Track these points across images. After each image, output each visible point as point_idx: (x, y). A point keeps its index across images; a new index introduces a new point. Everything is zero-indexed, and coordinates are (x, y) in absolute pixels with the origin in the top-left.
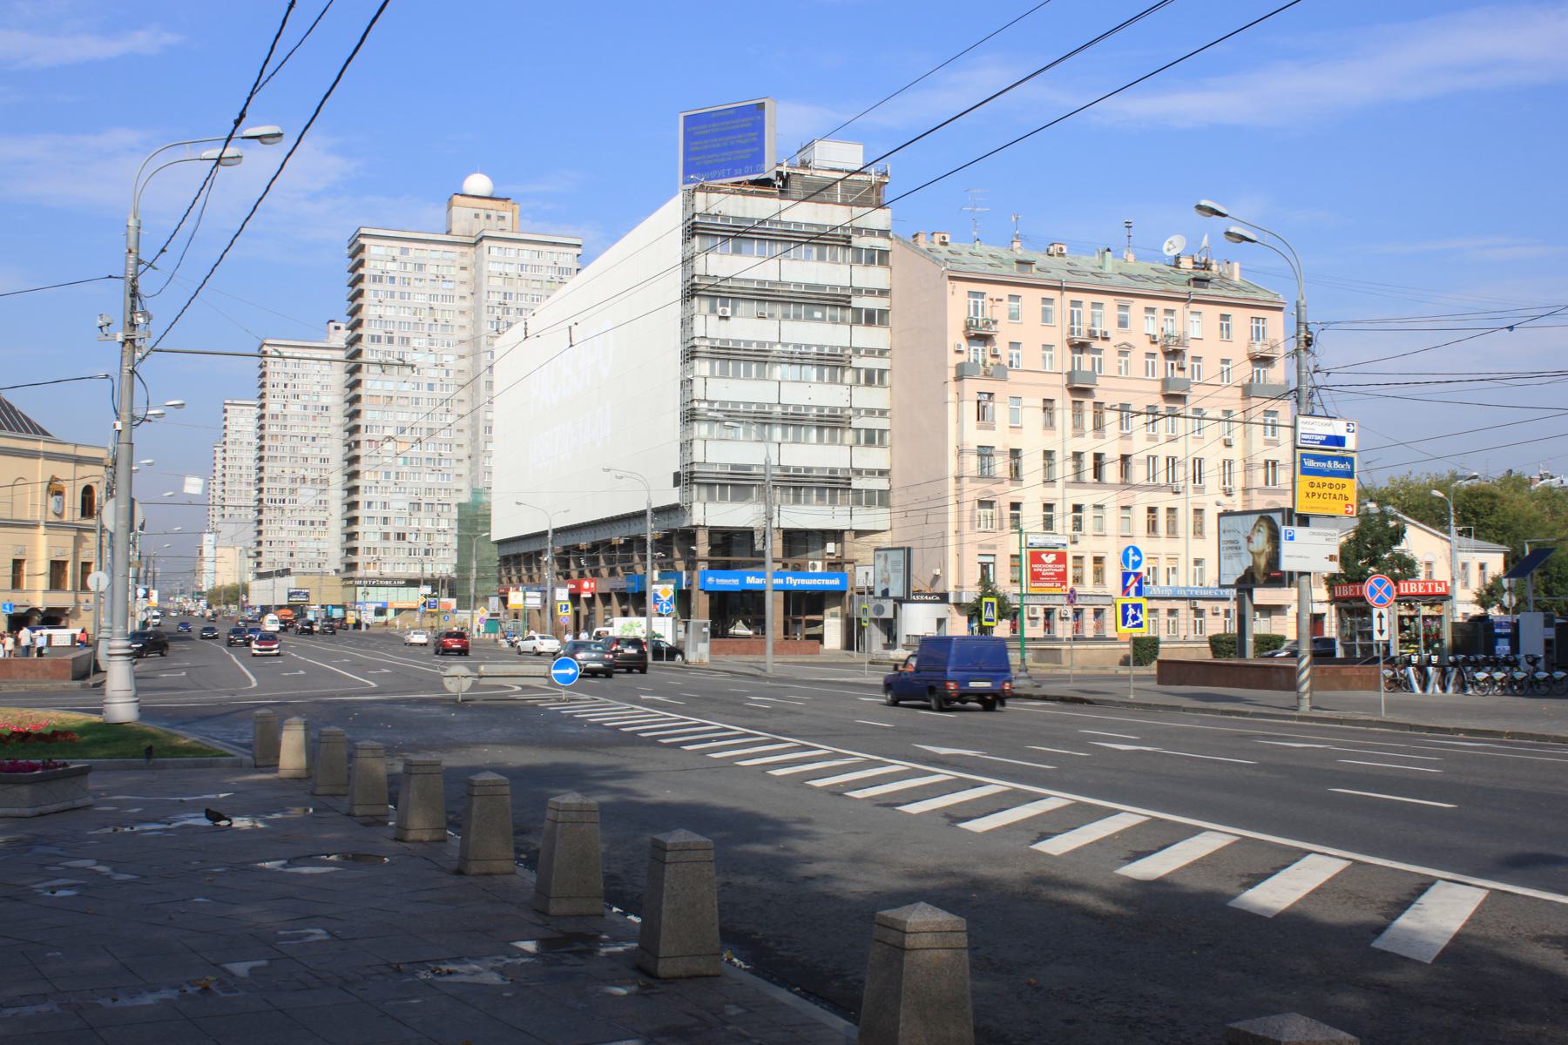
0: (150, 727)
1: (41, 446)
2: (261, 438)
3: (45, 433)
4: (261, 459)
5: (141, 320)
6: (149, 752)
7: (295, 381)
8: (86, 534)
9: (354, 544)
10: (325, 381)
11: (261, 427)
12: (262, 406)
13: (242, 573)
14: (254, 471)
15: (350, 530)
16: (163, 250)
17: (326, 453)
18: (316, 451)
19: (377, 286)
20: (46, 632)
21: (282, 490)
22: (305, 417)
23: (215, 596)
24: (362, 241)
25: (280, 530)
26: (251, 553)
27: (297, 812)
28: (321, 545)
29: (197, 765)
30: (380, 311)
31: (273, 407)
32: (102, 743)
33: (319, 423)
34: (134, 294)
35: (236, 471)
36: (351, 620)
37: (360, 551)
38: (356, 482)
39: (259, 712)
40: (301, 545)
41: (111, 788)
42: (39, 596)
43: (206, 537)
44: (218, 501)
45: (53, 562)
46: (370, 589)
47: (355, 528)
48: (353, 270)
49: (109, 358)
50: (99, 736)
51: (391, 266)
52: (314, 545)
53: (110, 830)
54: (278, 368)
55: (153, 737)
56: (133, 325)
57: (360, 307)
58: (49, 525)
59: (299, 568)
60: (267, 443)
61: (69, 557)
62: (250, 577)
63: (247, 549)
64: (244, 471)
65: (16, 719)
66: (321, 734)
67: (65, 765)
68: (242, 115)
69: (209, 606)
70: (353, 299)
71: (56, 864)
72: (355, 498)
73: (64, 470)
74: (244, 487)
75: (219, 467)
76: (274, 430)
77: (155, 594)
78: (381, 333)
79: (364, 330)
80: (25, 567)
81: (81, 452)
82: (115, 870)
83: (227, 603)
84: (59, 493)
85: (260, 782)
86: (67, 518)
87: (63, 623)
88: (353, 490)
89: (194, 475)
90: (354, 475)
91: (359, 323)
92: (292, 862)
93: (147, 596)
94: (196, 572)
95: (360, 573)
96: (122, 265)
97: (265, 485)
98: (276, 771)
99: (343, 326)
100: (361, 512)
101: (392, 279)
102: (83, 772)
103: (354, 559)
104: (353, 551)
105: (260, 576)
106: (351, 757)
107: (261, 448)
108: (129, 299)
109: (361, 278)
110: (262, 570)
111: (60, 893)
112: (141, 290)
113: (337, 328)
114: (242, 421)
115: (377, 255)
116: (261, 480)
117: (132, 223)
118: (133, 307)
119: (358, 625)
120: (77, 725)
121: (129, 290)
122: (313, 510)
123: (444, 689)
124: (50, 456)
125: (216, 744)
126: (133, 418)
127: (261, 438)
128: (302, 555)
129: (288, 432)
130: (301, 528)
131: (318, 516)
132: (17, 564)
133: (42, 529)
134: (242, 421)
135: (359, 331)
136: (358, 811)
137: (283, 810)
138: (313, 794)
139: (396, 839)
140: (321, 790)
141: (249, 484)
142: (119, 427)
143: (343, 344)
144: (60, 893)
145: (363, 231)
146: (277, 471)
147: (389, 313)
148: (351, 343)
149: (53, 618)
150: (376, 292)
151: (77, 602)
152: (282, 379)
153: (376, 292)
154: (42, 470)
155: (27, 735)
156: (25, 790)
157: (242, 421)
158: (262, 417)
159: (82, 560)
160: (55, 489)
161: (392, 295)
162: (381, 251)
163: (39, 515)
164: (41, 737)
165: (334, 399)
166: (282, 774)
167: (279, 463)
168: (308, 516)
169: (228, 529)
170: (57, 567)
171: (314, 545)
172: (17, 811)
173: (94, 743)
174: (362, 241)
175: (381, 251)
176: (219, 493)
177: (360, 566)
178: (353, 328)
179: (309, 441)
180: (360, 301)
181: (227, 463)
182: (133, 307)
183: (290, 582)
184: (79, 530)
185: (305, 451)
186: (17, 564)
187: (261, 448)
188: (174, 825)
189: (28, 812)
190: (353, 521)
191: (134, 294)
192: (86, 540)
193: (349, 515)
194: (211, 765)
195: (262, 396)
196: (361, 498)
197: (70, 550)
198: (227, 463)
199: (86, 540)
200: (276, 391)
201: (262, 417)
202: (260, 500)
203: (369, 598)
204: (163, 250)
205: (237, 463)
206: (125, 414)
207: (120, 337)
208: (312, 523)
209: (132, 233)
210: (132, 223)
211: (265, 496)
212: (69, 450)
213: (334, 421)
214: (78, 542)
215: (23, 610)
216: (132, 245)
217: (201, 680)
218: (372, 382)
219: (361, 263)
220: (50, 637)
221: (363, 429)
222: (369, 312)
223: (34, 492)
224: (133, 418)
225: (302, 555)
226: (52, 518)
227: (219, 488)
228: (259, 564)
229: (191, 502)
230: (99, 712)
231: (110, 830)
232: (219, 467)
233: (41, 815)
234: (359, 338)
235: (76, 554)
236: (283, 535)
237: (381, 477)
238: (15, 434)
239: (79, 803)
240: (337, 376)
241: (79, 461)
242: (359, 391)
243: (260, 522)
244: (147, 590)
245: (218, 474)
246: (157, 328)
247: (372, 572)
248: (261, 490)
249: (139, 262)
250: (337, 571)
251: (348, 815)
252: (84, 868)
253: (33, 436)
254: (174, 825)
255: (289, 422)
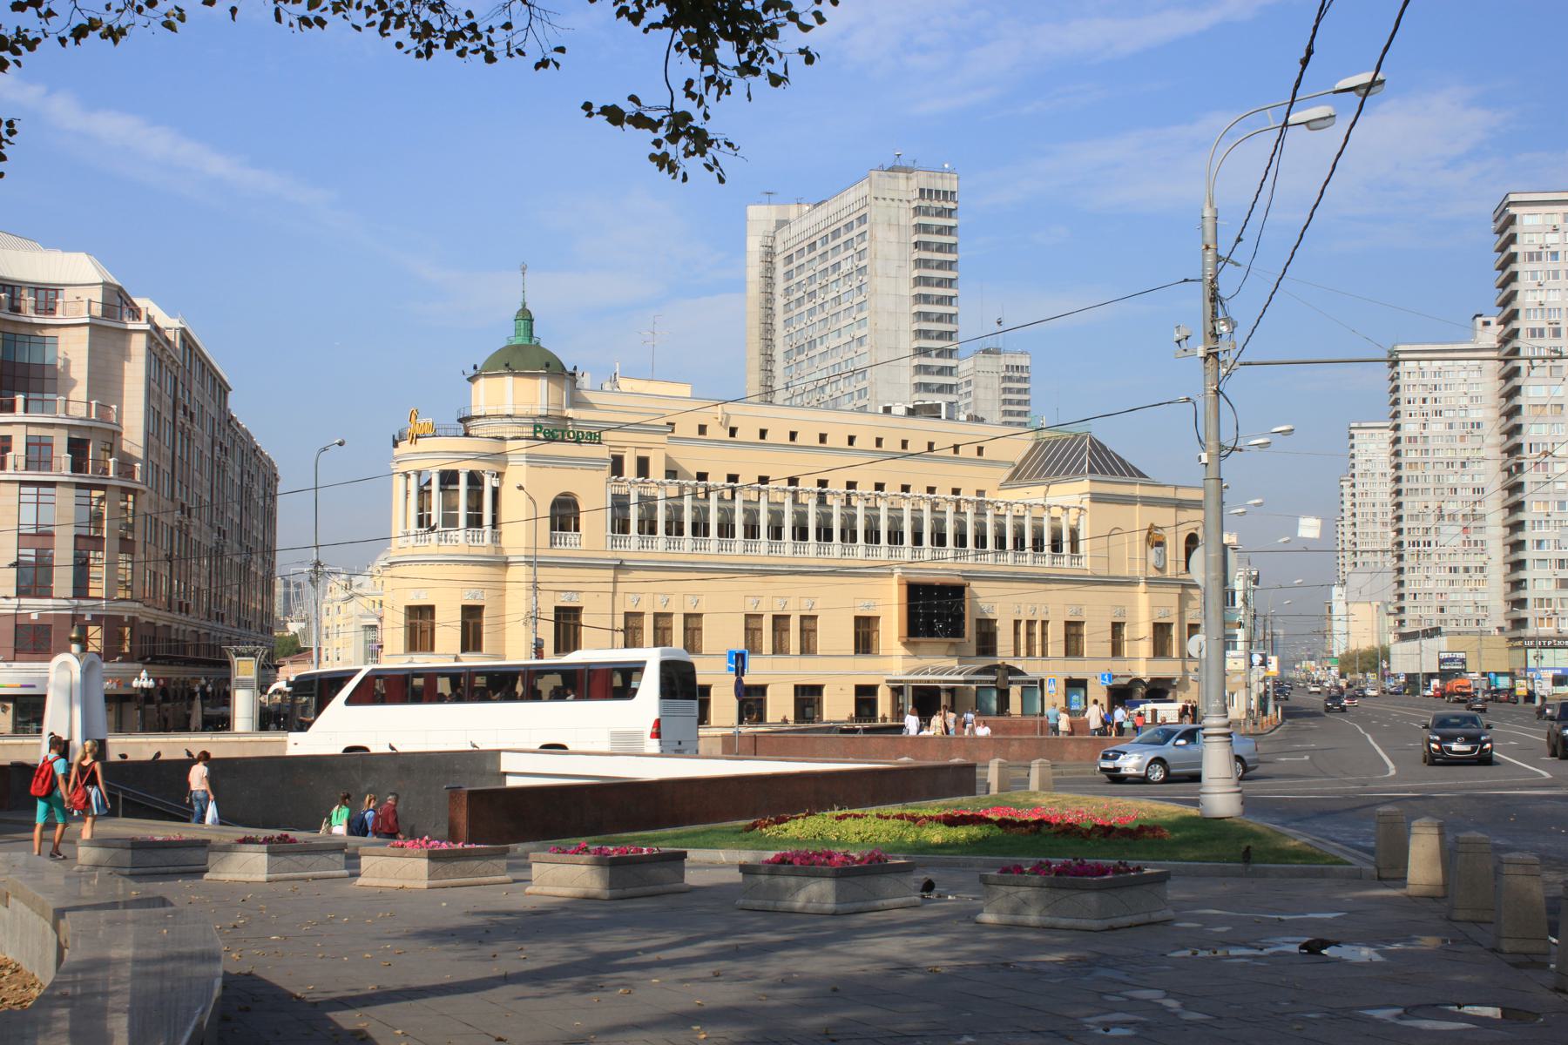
0: (1256, 824)
1: (1138, 490)
2: (1398, 467)
3: (1142, 475)
4: (1398, 492)
5: (1224, 329)
6: (1247, 856)
7: (1436, 394)
8: (1192, 591)
9: (1522, 594)
10: (1474, 391)
11: (1397, 454)
12: (1397, 428)
13: (1381, 634)
14: (1390, 508)
15: (1515, 577)
16: (1239, 240)
17: (1480, 481)
18: (1467, 479)
19: (1535, 266)
20: (1150, 706)
21: (1427, 530)
22: (1452, 438)
23: (1349, 662)
24: (1512, 210)
25: (1426, 580)
26: (1391, 609)
27: (1429, 942)
28: (1479, 597)
29: (1306, 874)
30: (1541, 296)
31: (1410, 428)
32: (1194, 842)
33: (1469, 444)
34: (1215, 298)
35: (1369, 509)
36: (1521, 691)
37: (1530, 603)
38: (1521, 516)
39: (1381, 809)
40: (1453, 597)
41: (1196, 899)
42: (1141, 664)
43: (1336, 590)
44: (1347, 546)
45: (1156, 625)
46: (1545, 652)
47: (1522, 575)
48: (1502, 249)
49: (1193, 378)
50: (1194, 832)
51: (1552, 238)
52: (1470, 597)
53: (1188, 953)
54: (1414, 379)
55: (1256, 836)
56: (1215, 336)
57: (1514, 294)
58: (1150, 582)
59: (1452, 627)
60: (1404, 472)
61: (1174, 619)
62: (1391, 638)
63: (1386, 604)
64: (1378, 509)
65: (1102, 810)
66: (1457, 841)
67: (1139, 869)
68: (1310, 52)
69: (1342, 676)
70: (1503, 286)
71: (1117, 993)
72: (1520, 536)
73: (1163, 517)
74: (1379, 529)
75: (1347, 505)
76: (1412, 456)
77: (1274, 661)
78: (1544, 325)
79: (1521, 324)
80: (1125, 631)
81: (1183, 495)
82: (1184, 1006)
83: (1364, 672)
84: (1160, 544)
85: (1383, 898)
86: (1170, 572)
87: (1170, 696)
88: (1518, 526)
89: (1309, 514)
90: (1517, 507)
91: (1514, 315)
92: (1409, 1012)
93: (1264, 663)
94: (1325, 634)
95: (1530, 631)
96: (1198, 264)
97: (1404, 525)
98: (1404, 886)
99: (1493, 321)
100: (1529, 554)
101: (1555, 255)
102: (1161, 879)
103: (1523, 614)
104: (1521, 603)
105: (1404, 637)
106: (1498, 873)
107: (1398, 479)
108: (1208, 304)
109: (1513, 258)
110: (1406, 630)
111: (1114, 1032)
112: (1221, 293)
113: (1487, 324)
114: (1372, 447)
115: (1532, 226)
116: (1399, 518)
117: (1208, 213)
118: (1215, 314)
119: (1530, 697)
120: (1171, 818)
121: (1209, 294)
122: (1466, 553)
123: (602, 861)
124: (1148, 501)
125: (1332, 848)
126: (1221, 447)
127: (1398, 467)
128: (1455, 611)
129: (1430, 457)
130: (1453, 576)
131: (1474, 561)
132: (1117, 628)
133: (1142, 587)
134: (1373, 447)
135: (1515, 325)
136: (1506, 946)
137: (1407, 939)
138: (1449, 919)
139: (1557, 990)
140: (1460, 915)
141: (1384, 524)
142: (1205, 459)
143: (1494, 343)
144: (1114, 1032)
145: (1512, 198)
146: (1419, 507)
147: (1553, 299)
148: (1504, 341)
149: (1159, 690)
150: (1534, 274)
151: (1185, 671)
152: (1418, 393)
153: (1534, 274)
154: (1140, 517)
155: (1111, 829)
156: (1092, 898)
157: (1373, 447)
158: (1397, 441)
159: (1188, 621)
160: (1155, 540)
161: (1556, 276)
162: (1537, 220)
163: (1138, 571)
164: (1126, 832)
165: (1487, 413)
166: (1411, 890)
167: (1420, 497)
168: (1460, 561)
169: (1355, 580)
170: (1161, 631)
171: (1470, 597)
172: (1084, 923)
173: (1184, 842)
174: (1512, 210)
175: (1537, 220)
176: (1348, 536)
177: (1531, 623)
178: (1505, 321)
179: (1457, 467)
180: (1513, 286)
181: (1357, 500)
182: (1215, 314)
183: (1441, 643)
184: (1184, 586)
185: (1452, 480)
186: (1117, 628)
187: (1398, 479)
188: (1266, 951)
189: (1095, 924)
190: (1519, 565)
191: (1215, 298)
192: (1192, 598)
193: (1513, 558)
194: (1322, 874)
195: (1396, 415)
196: (1528, 535)
197: (1175, 610)
198: (1357, 500)
199: (1192, 598)
200: (1412, 408)
201: (1397, 441)
202: (1400, 544)
203: (1544, 663)
204: (1239, 240)
205: (1369, 500)
206: (1212, 443)
207: (1201, 352)
208: (1467, 570)
209: (1209, 225)
210: (1208, 213)
211: (1405, 538)
212: (1168, 493)
213: (1489, 441)
214: (1183, 600)
215: (1125, 681)
216: (1209, 239)
217: (1308, 772)
218: (1534, 390)
219: (1512, 239)
220: (1154, 712)
221: (1526, 448)
222: (1526, 298)
223: (1132, 542)
224: (1221, 447)
225: (1455, 611)
226: (1153, 573)
227: (1348, 530)
228: (1401, 622)
229: (1307, 547)
230: (1196, 803)
231: (1188, 953)
232: (1347, 505)
233: (1112, 929)
234: (1515, 333)
235: (1181, 613)
236: (1430, 585)
237: (1553, 508)
238: (1104, 478)
239: (1156, 916)
240: (1485, 381)
241: (1180, 505)
242: (1518, 400)
243: (1400, 571)
244: (1264, 657)
245: (1347, 514)
246: (1241, 335)
247: (1547, 630)
248: (1399, 531)
249: (1218, 259)
250: (1501, 629)
251: (1494, 950)
252: (1148, 1001)
253: (1128, 479)
254: (1266, 951)
255: (1431, 445)
